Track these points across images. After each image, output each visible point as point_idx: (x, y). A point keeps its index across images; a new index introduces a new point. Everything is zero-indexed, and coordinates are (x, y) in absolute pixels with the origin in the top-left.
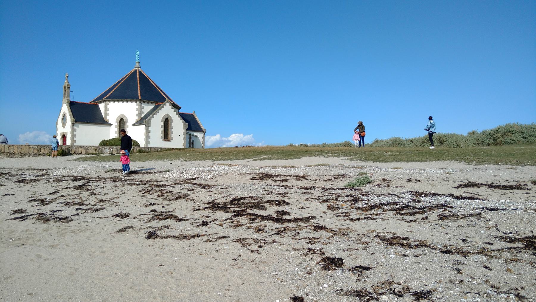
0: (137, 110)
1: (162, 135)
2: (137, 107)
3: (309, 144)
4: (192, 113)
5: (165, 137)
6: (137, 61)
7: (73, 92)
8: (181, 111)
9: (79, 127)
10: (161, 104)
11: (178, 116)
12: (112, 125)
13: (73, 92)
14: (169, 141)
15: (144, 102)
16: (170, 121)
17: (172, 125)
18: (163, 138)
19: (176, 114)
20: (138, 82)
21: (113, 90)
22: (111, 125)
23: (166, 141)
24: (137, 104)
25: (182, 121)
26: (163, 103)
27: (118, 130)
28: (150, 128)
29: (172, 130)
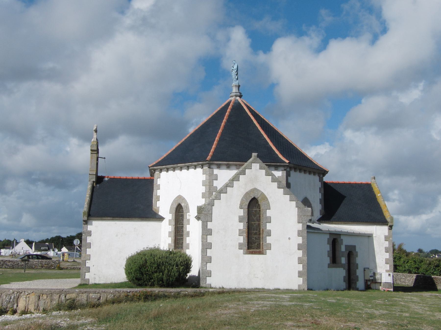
0: (204, 184)
1: (242, 239)
2: (204, 177)
3: (308, 155)
4: (369, 181)
5: (250, 245)
6: (235, 83)
7: (105, 158)
8: (326, 179)
9: (90, 230)
10: (243, 165)
11: (203, 192)
12: (164, 218)
13: (105, 158)
14: (261, 253)
15: (219, 167)
16: (160, 220)
17: (269, 213)
18: (246, 248)
19: (279, 187)
20: (223, 124)
21: (270, 164)
22: (161, 219)
23: (252, 253)
24: (203, 171)
25: (294, 203)
26: (246, 164)
27: (173, 229)
28: (210, 225)
29: (269, 226)
